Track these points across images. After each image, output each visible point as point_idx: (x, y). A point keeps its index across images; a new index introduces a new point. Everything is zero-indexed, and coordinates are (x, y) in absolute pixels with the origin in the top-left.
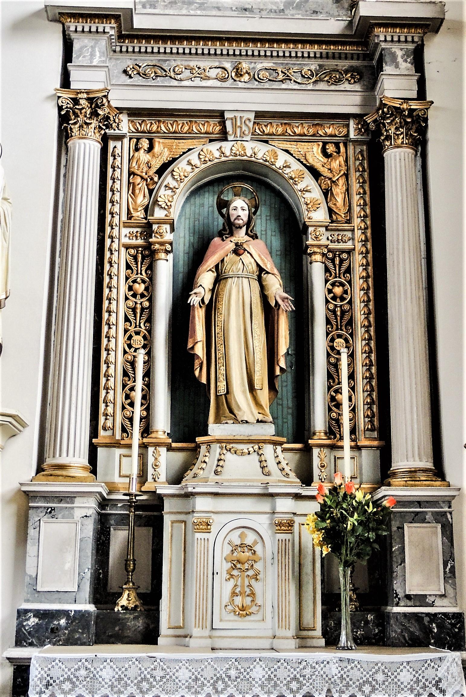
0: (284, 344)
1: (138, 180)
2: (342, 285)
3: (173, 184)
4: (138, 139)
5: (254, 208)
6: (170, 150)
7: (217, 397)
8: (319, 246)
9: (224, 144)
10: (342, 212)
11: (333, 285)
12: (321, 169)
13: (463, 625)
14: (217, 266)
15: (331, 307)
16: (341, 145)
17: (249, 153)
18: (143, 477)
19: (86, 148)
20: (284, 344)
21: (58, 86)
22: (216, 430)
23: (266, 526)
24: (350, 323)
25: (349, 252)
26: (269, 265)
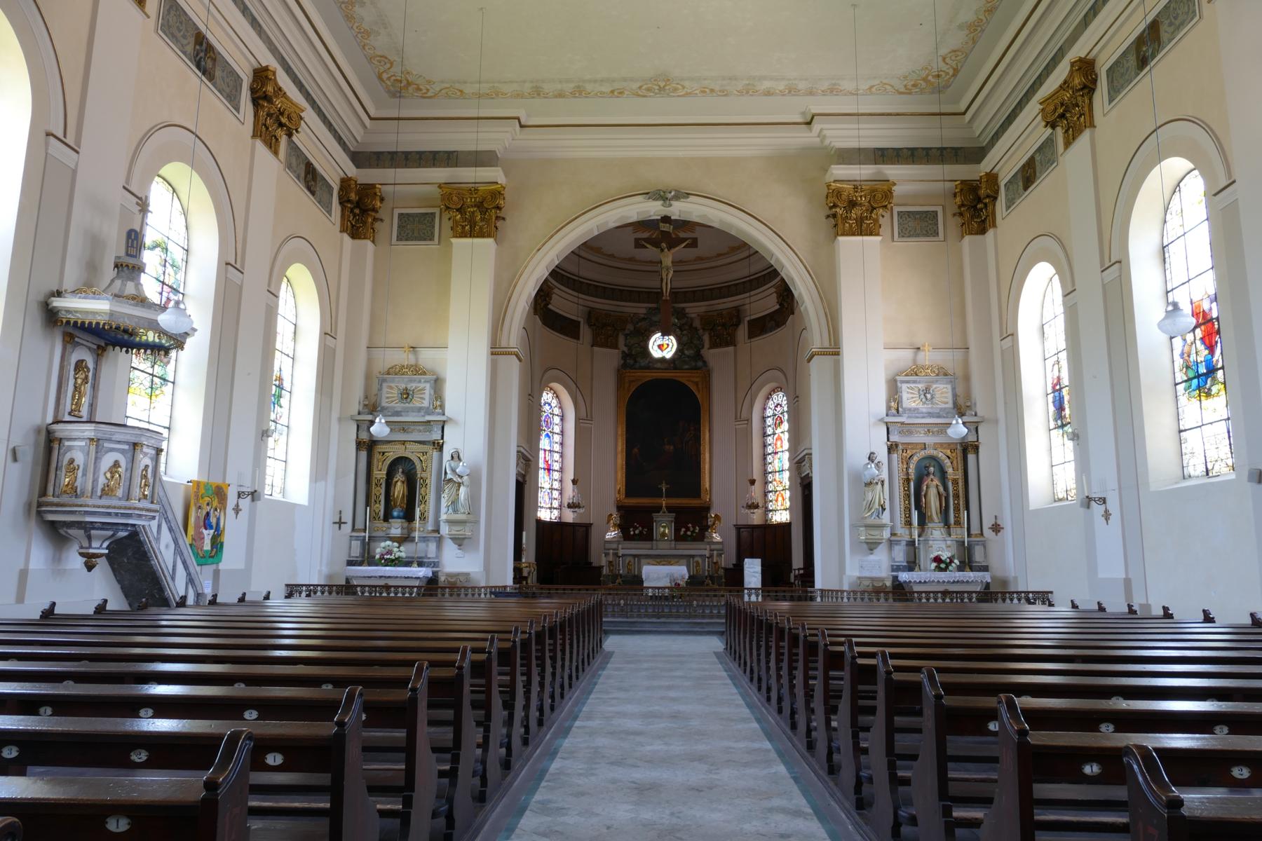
19: (364, 454)
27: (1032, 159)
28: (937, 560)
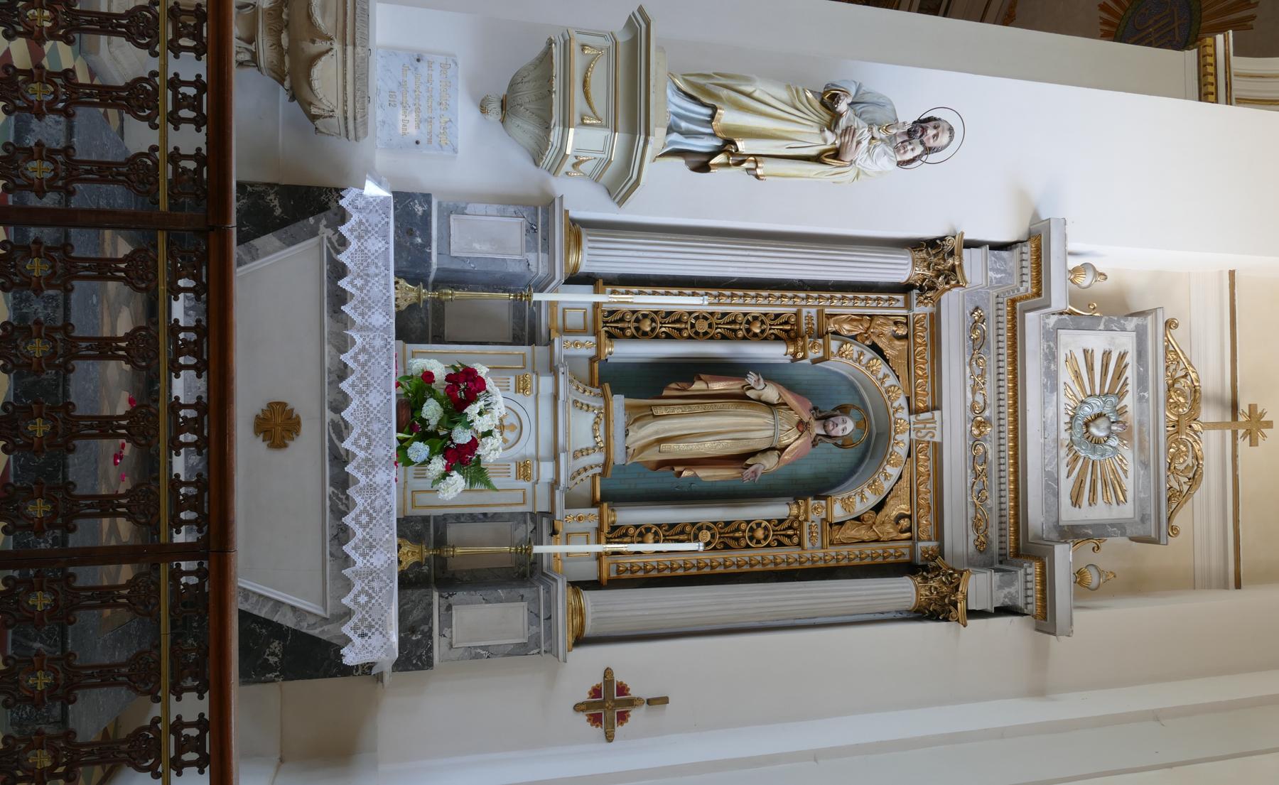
0: (706, 475)
1: (866, 325)
2: (766, 538)
3: (864, 360)
4: (906, 324)
5: (844, 443)
6: (896, 357)
7: (650, 407)
8: (806, 512)
9: (906, 410)
10: (838, 536)
11: (766, 528)
12: (882, 513)
13: (419, 669)
14: (785, 404)
15: (743, 526)
16: (908, 535)
17: (899, 437)
18: (566, 331)
19: (901, 269)
20: (706, 475)
21: (966, 237)
22: (618, 402)
23: (523, 451)
24: (727, 547)
25: (800, 544)
26: (786, 456)
27: (283, 603)
28: (465, 387)
